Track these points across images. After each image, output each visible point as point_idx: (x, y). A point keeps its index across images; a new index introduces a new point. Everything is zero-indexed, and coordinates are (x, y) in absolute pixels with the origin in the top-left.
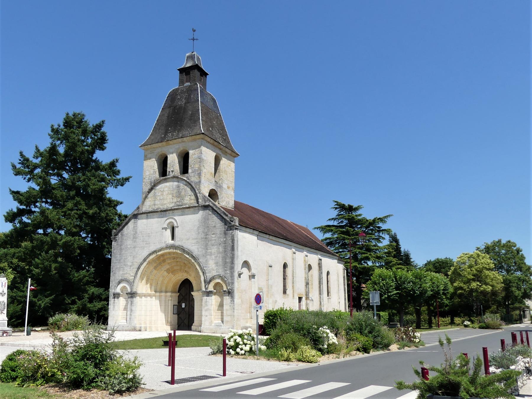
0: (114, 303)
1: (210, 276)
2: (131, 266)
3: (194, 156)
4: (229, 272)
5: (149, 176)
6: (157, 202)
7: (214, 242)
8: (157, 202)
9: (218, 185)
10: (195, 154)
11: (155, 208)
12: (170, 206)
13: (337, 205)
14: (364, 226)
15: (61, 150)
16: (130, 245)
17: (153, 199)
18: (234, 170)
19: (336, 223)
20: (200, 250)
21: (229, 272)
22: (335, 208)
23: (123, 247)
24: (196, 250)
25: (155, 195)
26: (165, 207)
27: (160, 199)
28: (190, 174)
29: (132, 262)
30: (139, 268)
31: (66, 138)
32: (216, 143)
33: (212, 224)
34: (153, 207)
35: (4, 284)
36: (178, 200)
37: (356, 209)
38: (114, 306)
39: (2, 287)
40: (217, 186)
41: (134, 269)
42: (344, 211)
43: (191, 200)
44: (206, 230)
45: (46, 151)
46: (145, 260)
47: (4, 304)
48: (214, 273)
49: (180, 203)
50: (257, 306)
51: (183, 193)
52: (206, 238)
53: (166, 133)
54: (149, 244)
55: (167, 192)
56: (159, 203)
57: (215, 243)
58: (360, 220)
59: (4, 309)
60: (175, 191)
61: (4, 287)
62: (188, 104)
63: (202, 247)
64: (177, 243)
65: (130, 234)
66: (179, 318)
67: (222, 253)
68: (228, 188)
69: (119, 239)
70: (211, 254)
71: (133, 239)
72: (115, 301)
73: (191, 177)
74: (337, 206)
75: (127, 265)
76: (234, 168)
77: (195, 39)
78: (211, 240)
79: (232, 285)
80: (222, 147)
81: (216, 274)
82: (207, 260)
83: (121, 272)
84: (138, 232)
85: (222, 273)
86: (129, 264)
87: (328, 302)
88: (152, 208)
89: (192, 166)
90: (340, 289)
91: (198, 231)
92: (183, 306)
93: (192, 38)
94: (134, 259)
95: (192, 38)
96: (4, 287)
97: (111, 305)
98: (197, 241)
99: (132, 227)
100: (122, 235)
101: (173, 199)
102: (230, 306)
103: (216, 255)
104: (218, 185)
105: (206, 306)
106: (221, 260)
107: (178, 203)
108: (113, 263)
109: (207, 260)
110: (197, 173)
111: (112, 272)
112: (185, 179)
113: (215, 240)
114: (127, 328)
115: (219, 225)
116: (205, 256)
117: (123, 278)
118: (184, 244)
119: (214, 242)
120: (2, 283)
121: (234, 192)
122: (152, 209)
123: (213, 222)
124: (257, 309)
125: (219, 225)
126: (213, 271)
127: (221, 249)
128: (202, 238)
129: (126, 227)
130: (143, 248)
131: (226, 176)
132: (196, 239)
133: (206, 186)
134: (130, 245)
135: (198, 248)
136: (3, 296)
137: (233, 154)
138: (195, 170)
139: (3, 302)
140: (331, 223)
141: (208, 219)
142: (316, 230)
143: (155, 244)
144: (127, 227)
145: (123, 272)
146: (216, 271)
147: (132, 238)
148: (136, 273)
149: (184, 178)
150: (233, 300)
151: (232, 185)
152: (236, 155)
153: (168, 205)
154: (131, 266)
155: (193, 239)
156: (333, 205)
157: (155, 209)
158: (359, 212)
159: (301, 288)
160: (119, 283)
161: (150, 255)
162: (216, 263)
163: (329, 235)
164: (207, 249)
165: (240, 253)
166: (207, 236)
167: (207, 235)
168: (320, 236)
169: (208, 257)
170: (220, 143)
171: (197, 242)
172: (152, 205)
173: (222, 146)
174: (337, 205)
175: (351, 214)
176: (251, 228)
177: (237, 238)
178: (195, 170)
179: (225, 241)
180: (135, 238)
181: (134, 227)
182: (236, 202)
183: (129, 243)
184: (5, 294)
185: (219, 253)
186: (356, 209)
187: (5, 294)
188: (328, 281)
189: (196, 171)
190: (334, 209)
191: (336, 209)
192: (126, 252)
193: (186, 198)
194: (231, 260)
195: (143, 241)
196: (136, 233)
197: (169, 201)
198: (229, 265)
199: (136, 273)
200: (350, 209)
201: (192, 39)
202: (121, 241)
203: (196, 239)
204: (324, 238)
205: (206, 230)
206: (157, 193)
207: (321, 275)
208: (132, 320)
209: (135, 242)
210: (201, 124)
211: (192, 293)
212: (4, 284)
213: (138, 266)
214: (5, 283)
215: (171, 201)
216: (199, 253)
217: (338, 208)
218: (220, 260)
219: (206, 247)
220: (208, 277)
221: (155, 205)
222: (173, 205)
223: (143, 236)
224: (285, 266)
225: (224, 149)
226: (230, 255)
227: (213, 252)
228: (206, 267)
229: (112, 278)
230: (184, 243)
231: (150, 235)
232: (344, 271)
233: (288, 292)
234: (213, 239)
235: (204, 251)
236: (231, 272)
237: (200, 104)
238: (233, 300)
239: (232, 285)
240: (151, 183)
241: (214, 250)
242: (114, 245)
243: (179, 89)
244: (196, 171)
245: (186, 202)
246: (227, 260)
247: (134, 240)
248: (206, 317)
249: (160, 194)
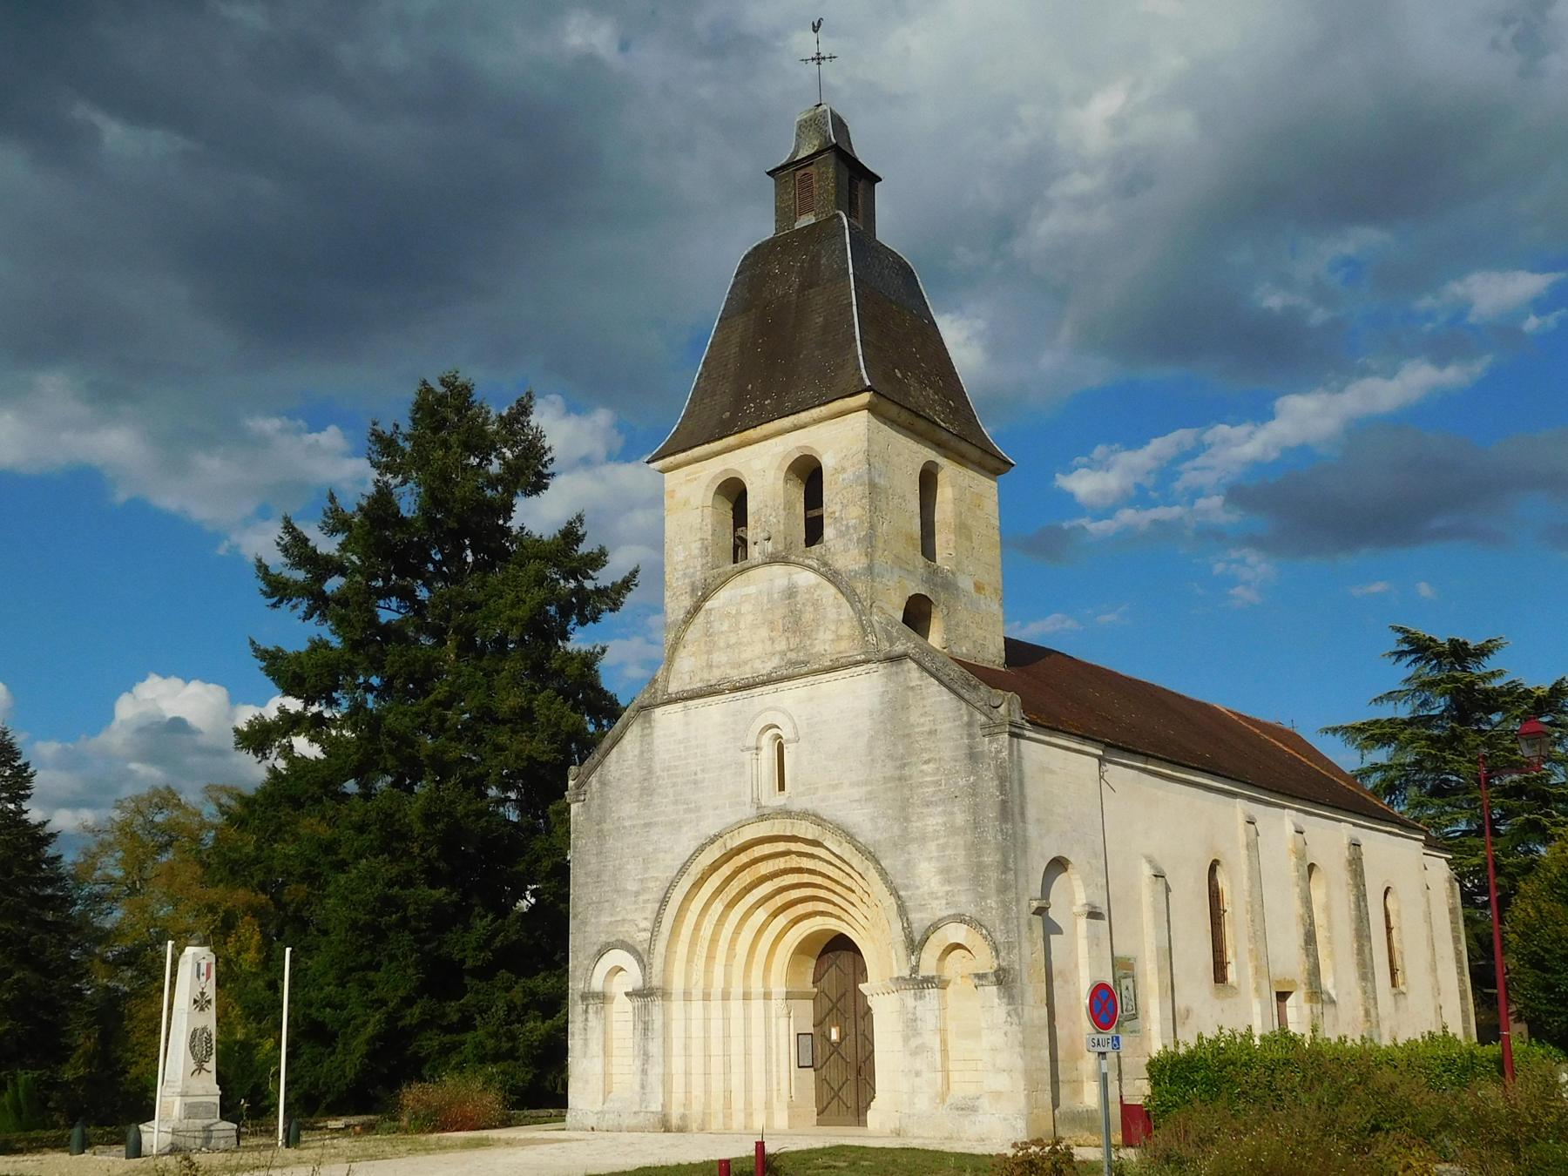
0: (585, 1029)
1: (922, 920)
2: (637, 894)
3: (841, 477)
4: (993, 905)
5: (684, 566)
6: (719, 657)
7: (931, 790)
8: (719, 657)
9: (940, 581)
10: (844, 469)
11: (714, 676)
12: (765, 668)
13: (1405, 640)
14: (1517, 716)
15: (408, 502)
16: (630, 817)
17: (702, 644)
18: (997, 523)
19: (1404, 711)
20: (882, 823)
21: (993, 905)
22: (1395, 653)
23: (605, 826)
24: (868, 826)
25: (708, 633)
26: (747, 673)
27: (728, 646)
28: (830, 544)
29: (642, 880)
30: (664, 902)
31: (421, 460)
32: (921, 425)
33: (923, 725)
34: (706, 676)
35: (203, 969)
36: (792, 640)
37: (1483, 652)
38: (586, 1040)
39: (198, 977)
40: (935, 585)
41: (649, 906)
42: (1434, 662)
43: (839, 638)
44: (901, 750)
45: (361, 508)
46: (683, 870)
47: (209, 1040)
48: (939, 909)
49: (802, 656)
50: (1101, 1036)
51: (808, 616)
52: (900, 779)
53: (739, 400)
54: (698, 809)
55: (750, 618)
56: (724, 659)
57: (934, 793)
58: (1499, 692)
59: (209, 1054)
60: (781, 611)
61: (203, 978)
62: (811, 291)
63: (890, 811)
64: (795, 797)
65: (629, 779)
66: (821, 1082)
67: (965, 833)
68: (979, 588)
69: (592, 798)
70: (923, 839)
71: (641, 795)
72: (589, 1024)
73: (834, 554)
74: (1406, 647)
75: (625, 890)
76: (997, 515)
77: (824, 58)
78: (921, 785)
79: (1008, 954)
80: (945, 436)
81: (945, 913)
82: (908, 861)
83: (605, 919)
84: (657, 767)
85: (970, 910)
86: (632, 886)
87: (1397, 1009)
88: (701, 680)
89: (837, 514)
90: (1437, 957)
91: (870, 753)
92: (834, 1035)
93: (822, 55)
94: (646, 870)
95: (815, 56)
96: (203, 978)
97: (576, 1037)
98: (870, 793)
99: (637, 752)
100: (603, 783)
101: (772, 640)
102: (1005, 1034)
103: (941, 841)
104: (940, 581)
105: (914, 1036)
106: (961, 860)
107: (792, 656)
108: (575, 885)
109: (908, 861)
110: (855, 537)
111: (575, 916)
112: (814, 564)
113: (938, 783)
114: (634, 1122)
115: (948, 725)
116: (903, 841)
117: (614, 939)
118: (823, 805)
119: (931, 790)
120: (199, 965)
121: (1001, 605)
122: (699, 685)
123: (925, 714)
124: (1101, 1049)
125: (948, 725)
126: (935, 903)
127: (960, 819)
128: (886, 780)
129: (615, 750)
130: (675, 826)
131: (968, 543)
132: (866, 783)
133: (890, 583)
134: (630, 817)
135: (872, 819)
136: (202, 1009)
137: (994, 463)
138: (848, 527)
139: (204, 1029)
140: (1386, 712)
141: (905, 707)
142: (1330, 735)
143: (717, 812)
144: (619, 753)
145: (612, 915)
146: (944, 902)
147: (637, 793)
148: (658, 921)
149: (808, 562)
150: (1015, 1010)
151: (993, 578)
152: (1002, 466)
153: (758, 664)
154: (637, 894)
155: (853, 785)
156: (1393, 642)
157: (713, 682)
158: (1489, 664)
159: (1288, 959)
160: (600, 954)
161: (701, 849)
162: (946, 873)
163: (1380, 755)
164: (907, 819)
165: (1032, 830)
166: (906, 771)
167: (905, 765)
168: (1347, 758)
169: (913, 847)
170: (935, 423)
171: (870, 798)
172: (702, 669)
173: (944, 433)
174: (1405, 640)
175: (1464, 670)
176: (1073, 730)
177: (1020, 771)
178: (848, 527)
179: (974, 786)
180: (647, 790)
181: (642, 752)
182: (1010, 644)
183: (626, 810)
184: (209, 1002)
185: (953, 830)
186: (1483, 652)
187: (209, 1002)
188: (1389, 929)
189: (852, 531)
190: (1394, 658)
191: (1398, 660)
192: (620, 845)
193: (821, 635)
194: (998, 857)
195: (676, 802)
196: (650, 771)
197: (758, 649)
198: (994, 875)
199: (658, 921)
200: (1459, 652)
201: (819, 64)
202: (601, 807)
203: (866, 783)
204: (1366, 765)
205: (901, 750)
206: (716, 625)
207: (1362, 904)
208: (648, 1090)
209: (648, 806)
210: (861, 358)
211: (861, 986)
212: (203, 969)
213: (662, 894)
214: (209, 966)
215: (769, 649)
216: (878, 837)
217: (1410, 652)
218: (960, 858)
219: (903, 811)
220: (915, 926)
221: (710, 666)
222: (775, 661)
223: (674, 785)
224: (1441, 1007)
225: (955, 442)
226: (995, 838)
227: (930, 829)
228: (906, 887)
229: (574, 941)
230: (823, 800)
231: (700, 776)
232: (1452, 887)
233: (1231, 973)
234: (928, 779)
235: (896, 830)
236: (1003, 901)
237: (853, 286)
238: (1015, 1010)
239: (1008, 954)
240: (693, 590)
241: (933, 821)
242: (576, 824)
243: (776, 242)
244: (852, 531)
245: (819, 647)
246: (987, 860)
247: (646, 798)
248: (918, 1079)
249: (725, 627)
